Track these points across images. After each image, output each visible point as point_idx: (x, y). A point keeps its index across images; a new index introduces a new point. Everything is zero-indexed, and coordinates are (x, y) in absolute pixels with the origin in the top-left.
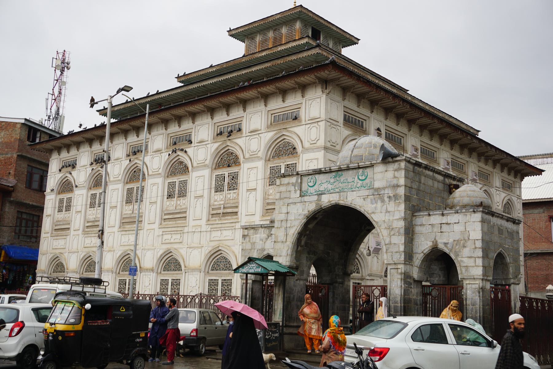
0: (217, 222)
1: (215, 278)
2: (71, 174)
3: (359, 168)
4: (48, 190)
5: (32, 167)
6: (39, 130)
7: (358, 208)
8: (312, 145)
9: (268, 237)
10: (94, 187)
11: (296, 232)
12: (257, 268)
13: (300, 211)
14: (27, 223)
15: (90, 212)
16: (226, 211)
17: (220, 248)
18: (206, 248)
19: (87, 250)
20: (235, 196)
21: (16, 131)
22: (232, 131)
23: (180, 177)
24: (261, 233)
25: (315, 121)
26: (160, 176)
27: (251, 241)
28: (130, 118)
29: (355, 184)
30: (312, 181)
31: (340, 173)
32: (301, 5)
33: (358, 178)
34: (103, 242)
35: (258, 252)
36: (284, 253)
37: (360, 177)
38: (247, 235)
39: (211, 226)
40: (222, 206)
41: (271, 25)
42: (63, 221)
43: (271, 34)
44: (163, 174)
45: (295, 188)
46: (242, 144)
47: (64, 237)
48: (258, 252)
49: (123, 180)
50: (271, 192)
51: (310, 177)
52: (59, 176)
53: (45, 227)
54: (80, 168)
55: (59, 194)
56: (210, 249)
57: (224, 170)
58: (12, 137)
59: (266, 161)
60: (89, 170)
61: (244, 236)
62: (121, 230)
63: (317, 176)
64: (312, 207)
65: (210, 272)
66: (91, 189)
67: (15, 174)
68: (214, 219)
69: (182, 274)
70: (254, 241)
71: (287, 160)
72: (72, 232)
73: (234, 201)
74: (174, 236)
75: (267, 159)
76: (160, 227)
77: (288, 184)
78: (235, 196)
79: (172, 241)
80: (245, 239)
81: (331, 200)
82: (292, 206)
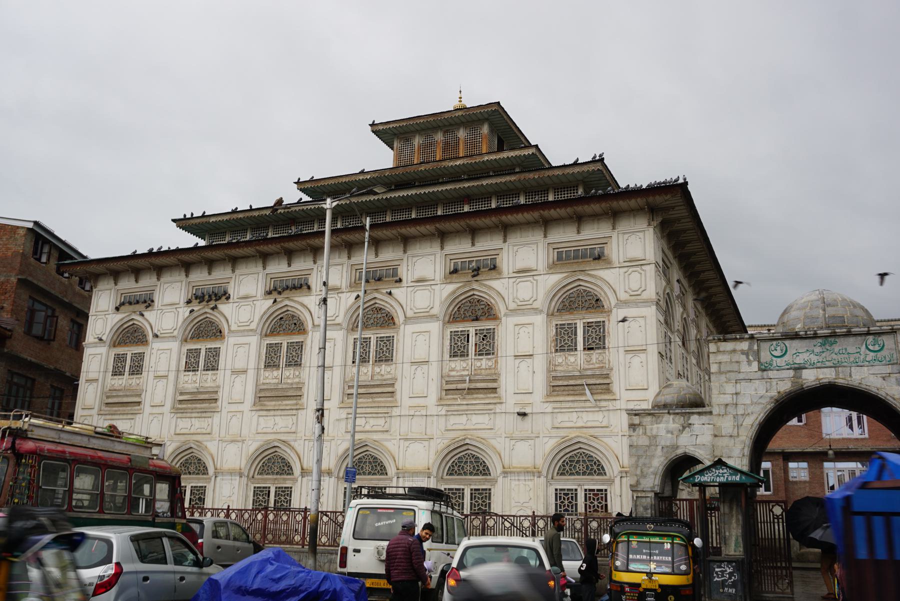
0: (459, 402)
1: (457, 487)
2: (143, 315)
3: (868, 333)
4: (90, 336)
5: (34, 300)
6: (49, 242)
7: (874, 390)
8: (633, 298)
9: (684, 428)
10: (192, 338)
11: (757, 422)
12: (731, 475)
13: (762, 392)
14: (17, 392)
15: (186, 378)
16: (473, 386)
17: (467, 441)
18: (250, 442)
19: (183, 438)
20: (490, 364)
21: (16, 239)
22: (478, 269)
23: (378, 331)
24: (667, 422)
25: (635, 263)
26: (339, 327)
27: (649, 434)
28: (231, 239)
29: (862, 357)
30: (778, 348)
31: (832, 339)
32: (499, 103)
33: (867, 348)
34: (323, 429)
35: (665, 450)
36: (737, 452)
37: (871, 347)
38: (639, 425)
39: (445, 408)
40: (467, 378)
41: (440, 124)
42: (125, 389)
43: (439, 137)
44: (345, 325)
45: (748, 358)
46: (500, 289)
47: (130, 416)
48: (665, 450)
49: (259, 331)
50: (560, 360)
51: (774, 343)
52: (115, 319)
53: (84, 399)
54: (163, 308)
55: (114, 346)
56: (446, 442)
57: (467, 324)
58: (8, 249)
59: (548, 315)
60: (184, 312)
61: (632, 426)
62: (258, 408)
63: (787, 343)
64: (786, 387)
65: (445, 477)
66: (186, 341)
67: (12, 310)
68: (449, 397)
69: (210, 479)
70: (654, 433)
71: (587, 316)
72: (147, 409)
73: (488, 372)
74: (372, 422)
75: (550, 312)
76: (341, 406)
77: (734, 351)
78: (490, 364)
79: (368, 428)
80: (634, 430)
81: (821, 377)
82: (743, 383)
